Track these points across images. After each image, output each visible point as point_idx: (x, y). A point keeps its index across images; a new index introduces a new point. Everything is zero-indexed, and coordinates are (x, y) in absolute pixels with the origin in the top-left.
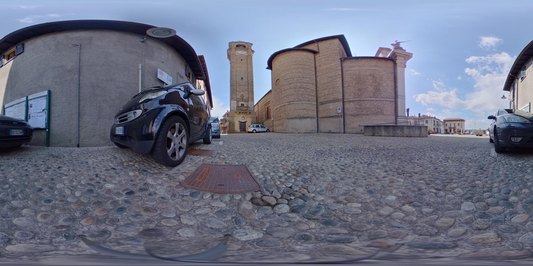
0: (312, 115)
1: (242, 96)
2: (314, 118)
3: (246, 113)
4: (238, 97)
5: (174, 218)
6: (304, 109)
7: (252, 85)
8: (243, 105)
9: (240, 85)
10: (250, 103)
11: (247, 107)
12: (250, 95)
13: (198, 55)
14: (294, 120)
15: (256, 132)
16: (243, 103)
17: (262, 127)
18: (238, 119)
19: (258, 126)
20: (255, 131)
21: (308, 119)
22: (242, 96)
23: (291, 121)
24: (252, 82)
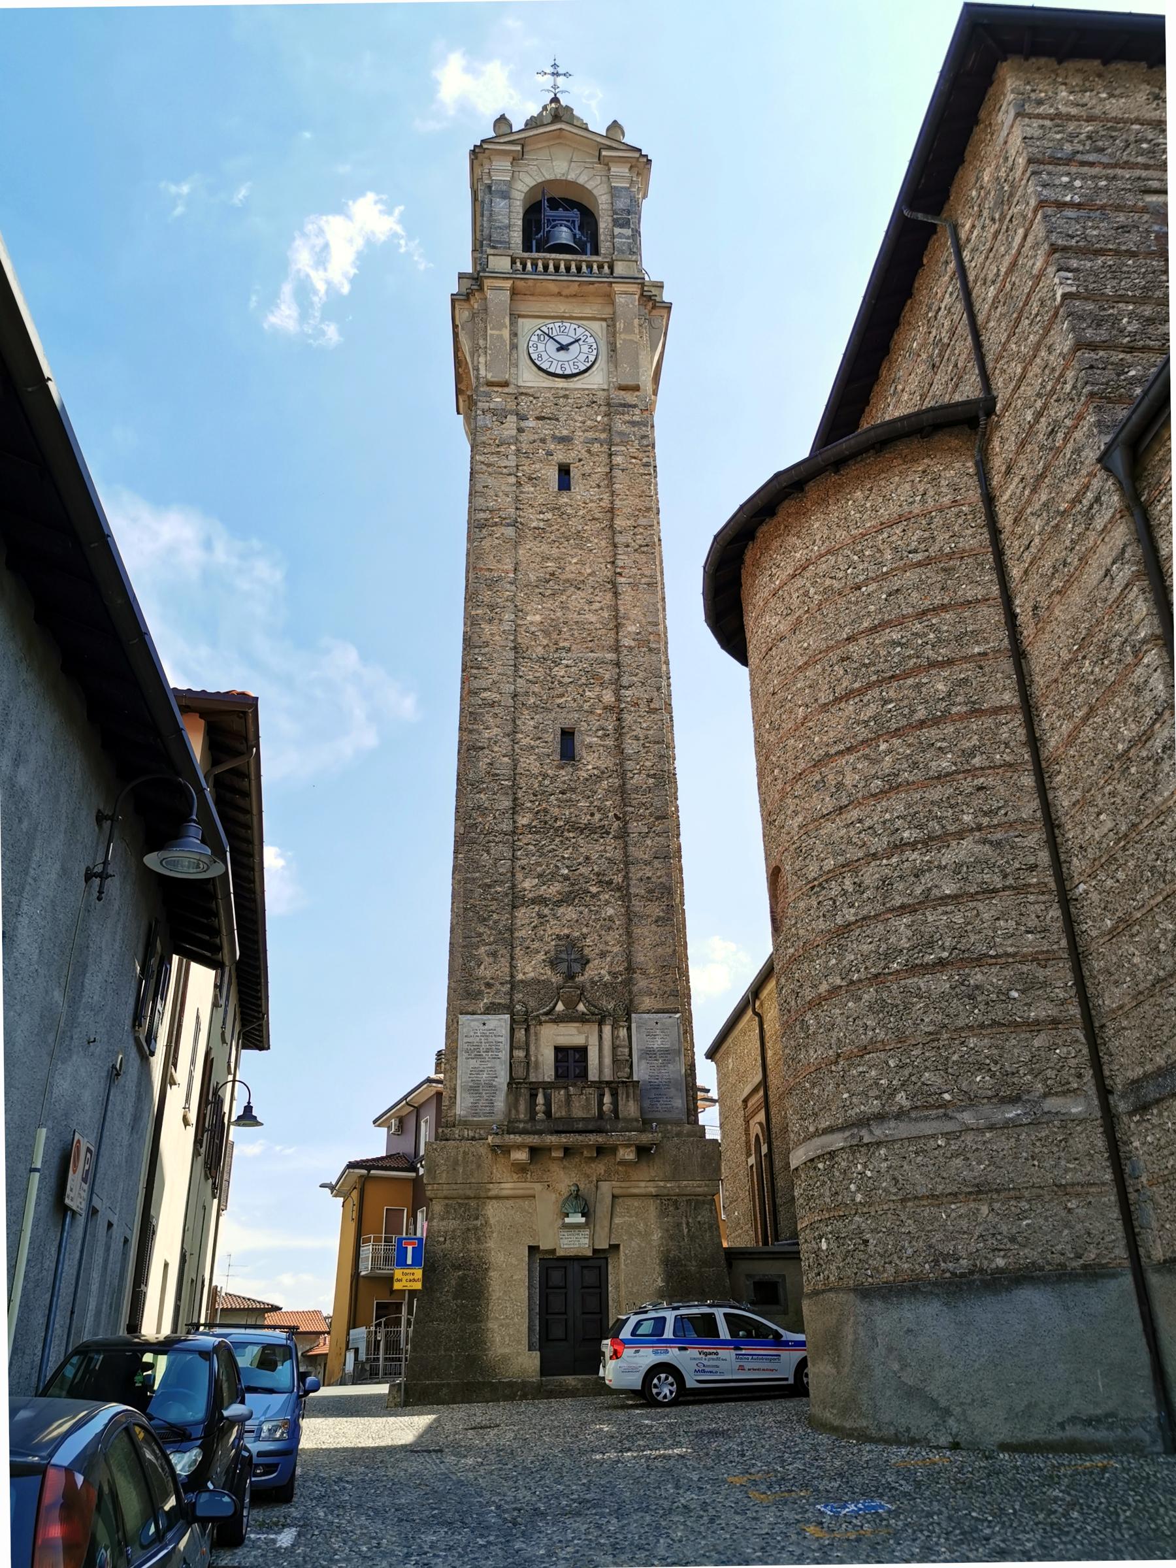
0: (1063, 1243)
1: (569, 957)
2: (1094, 1273)
4: (530, 968)
5: (637, 862)
6: (980, 1190)
7: (665, 820)
8: (571, 1060)
9: (545, 827)
10: (648, 1032)
11: (621, 1085)
12: (646, 933)
13: (176, 680)
14: (909, 1312)
15: (686, 1396)
16: (571, 1035)
17: (747, 1334)
18: (525, 1220)
19: (705, 1329)
20: (666, 1390)
21: (1031, 1297)
22: (569, 957)
23: (890, 1319)
24: (665, 780)
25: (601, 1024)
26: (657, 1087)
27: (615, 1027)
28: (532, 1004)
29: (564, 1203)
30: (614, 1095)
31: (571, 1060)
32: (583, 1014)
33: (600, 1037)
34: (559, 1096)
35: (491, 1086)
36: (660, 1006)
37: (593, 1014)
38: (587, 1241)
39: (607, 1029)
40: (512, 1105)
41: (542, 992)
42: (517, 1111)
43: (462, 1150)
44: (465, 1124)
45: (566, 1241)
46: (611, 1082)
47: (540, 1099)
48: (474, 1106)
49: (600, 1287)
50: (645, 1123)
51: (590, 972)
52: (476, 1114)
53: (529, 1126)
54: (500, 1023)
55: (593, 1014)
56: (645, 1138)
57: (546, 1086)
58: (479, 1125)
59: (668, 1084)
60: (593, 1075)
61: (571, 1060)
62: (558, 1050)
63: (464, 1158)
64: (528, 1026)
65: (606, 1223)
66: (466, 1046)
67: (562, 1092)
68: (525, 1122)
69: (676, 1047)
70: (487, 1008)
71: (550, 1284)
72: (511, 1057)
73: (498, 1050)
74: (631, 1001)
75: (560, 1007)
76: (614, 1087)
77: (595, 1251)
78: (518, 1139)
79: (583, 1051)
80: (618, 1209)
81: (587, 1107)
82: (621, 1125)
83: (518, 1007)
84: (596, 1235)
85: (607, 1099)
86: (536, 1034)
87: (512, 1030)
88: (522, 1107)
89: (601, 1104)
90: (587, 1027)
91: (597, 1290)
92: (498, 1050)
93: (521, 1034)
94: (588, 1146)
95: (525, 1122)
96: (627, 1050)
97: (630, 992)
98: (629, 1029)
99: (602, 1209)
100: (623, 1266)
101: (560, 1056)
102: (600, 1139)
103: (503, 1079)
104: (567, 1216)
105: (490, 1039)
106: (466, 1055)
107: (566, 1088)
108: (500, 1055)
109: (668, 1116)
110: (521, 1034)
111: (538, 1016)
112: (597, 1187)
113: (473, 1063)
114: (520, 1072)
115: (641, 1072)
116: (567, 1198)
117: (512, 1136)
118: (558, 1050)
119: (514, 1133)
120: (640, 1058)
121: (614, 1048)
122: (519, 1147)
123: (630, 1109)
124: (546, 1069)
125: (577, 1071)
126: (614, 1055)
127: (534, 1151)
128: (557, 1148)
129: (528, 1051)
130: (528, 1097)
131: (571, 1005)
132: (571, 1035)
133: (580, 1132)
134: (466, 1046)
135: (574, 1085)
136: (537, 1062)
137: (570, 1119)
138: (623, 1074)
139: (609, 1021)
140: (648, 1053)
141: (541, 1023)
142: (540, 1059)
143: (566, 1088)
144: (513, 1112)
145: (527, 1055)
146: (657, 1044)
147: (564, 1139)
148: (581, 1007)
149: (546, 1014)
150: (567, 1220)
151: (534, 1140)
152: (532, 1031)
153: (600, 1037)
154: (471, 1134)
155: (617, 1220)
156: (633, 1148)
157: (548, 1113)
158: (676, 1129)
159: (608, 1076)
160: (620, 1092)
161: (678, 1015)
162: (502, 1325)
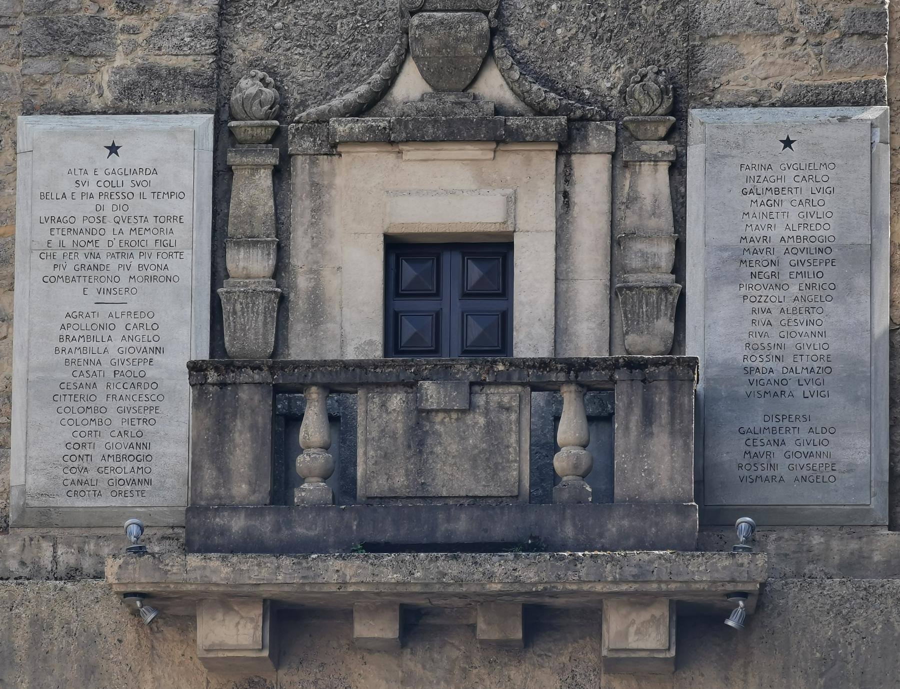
3: (542, 621)
8: (446, 286)
16: (447, 192)
25: (566, 147)
26: (777, 390)
27: (620, 162)
28: (303, 72)
30: (600, 419)
31: (446, 286)
32: (499, 110)
33: (565, 200)
34: (381, 416)
35: (139, 382)
36: (804, 76)
37: (539, 110)
39: (592, 170)
40: (210, 446)
41: (343, 27)
42: (223, 471)
43: (25, 614)
44: (44, 520)
46: (588, 364)
47: (313, 427)
48: (77, 453)
50: (713, 524)
52: (81, 486)
53: (265, 526)
54: (175, 147)
55: (539, 110)
56: (705, 572)
57: (343, 381)
58: (99, 526)
59: (821, 374)
60: (531, 339)
61: (451, 288)
62: (399, 249)
63: (35, 642)
64: (286, 159)
66: (42, 234)
67: (397, 400)
68: (255, 511)
69: (861, 235)
70: (128, 90)
72: (218, 274)
73: (169, 249)
74: (692, 58)
75: (411, 85)
76: (597, 383)
78: (217, 570)
79: (494, 253)
81: (491, 456)
82: (616, 524)
83: (248, 86)
85: (571, 426)
86: (317, 189)
87: (222, 177)
88: (244, 450)
89: (545, 446)
90: (510, 163)
92: (169, 249)
93: (254, 190)
94: (488, 600)
95: (255, 511)
96: (664, 250)
97: (689, 25)
98: (677, 168)
101: (409, 272)
102: (529, 572)
103: (185, 338)
105: (137, 207)
106: (45, 267)
107: (411, 385)
108: (175, 266)
109: (811, 497)
110: (254, 190)
111: (322, 120)
113: (73, 297)
114: (251, 333)
115: (717, 332)
117: (194, 560)
118: (399, 249)
119: (205, 549)
120: (714, 280)
121: (617, 240)
122: (229, 600)
123: (656, 464)
124: (351, 314)
125: (475, 330)
126: (615, 267)
127: (291, 622)
128: (376, 602)
129: (282, 252)
130: (263, 419)
131: (453, 75)
132: (447, 192)
133: (453, 548)
134: (42, 234)
135: (443, 374)
136: (317, 299)
137: (425, 501)
138: (647, 342)
139: (600, 138)
140: (748, 261)
141: (333, 148)
142: (332, 284)
143: (411, 385)
144: (209, 473)
145: (281, 270)
146: (784, 224)
147: (389, 571)
148: (493, 86)
149: (359, 110)
151: (278, 574)
152: (301, 170)
153: (565, 200)
154: (67, 557)
156: (661, 611)
157: (342, 476)
158: (841, 547)
159: (588, 340)
160: (620, 403)
161: (874, 113)
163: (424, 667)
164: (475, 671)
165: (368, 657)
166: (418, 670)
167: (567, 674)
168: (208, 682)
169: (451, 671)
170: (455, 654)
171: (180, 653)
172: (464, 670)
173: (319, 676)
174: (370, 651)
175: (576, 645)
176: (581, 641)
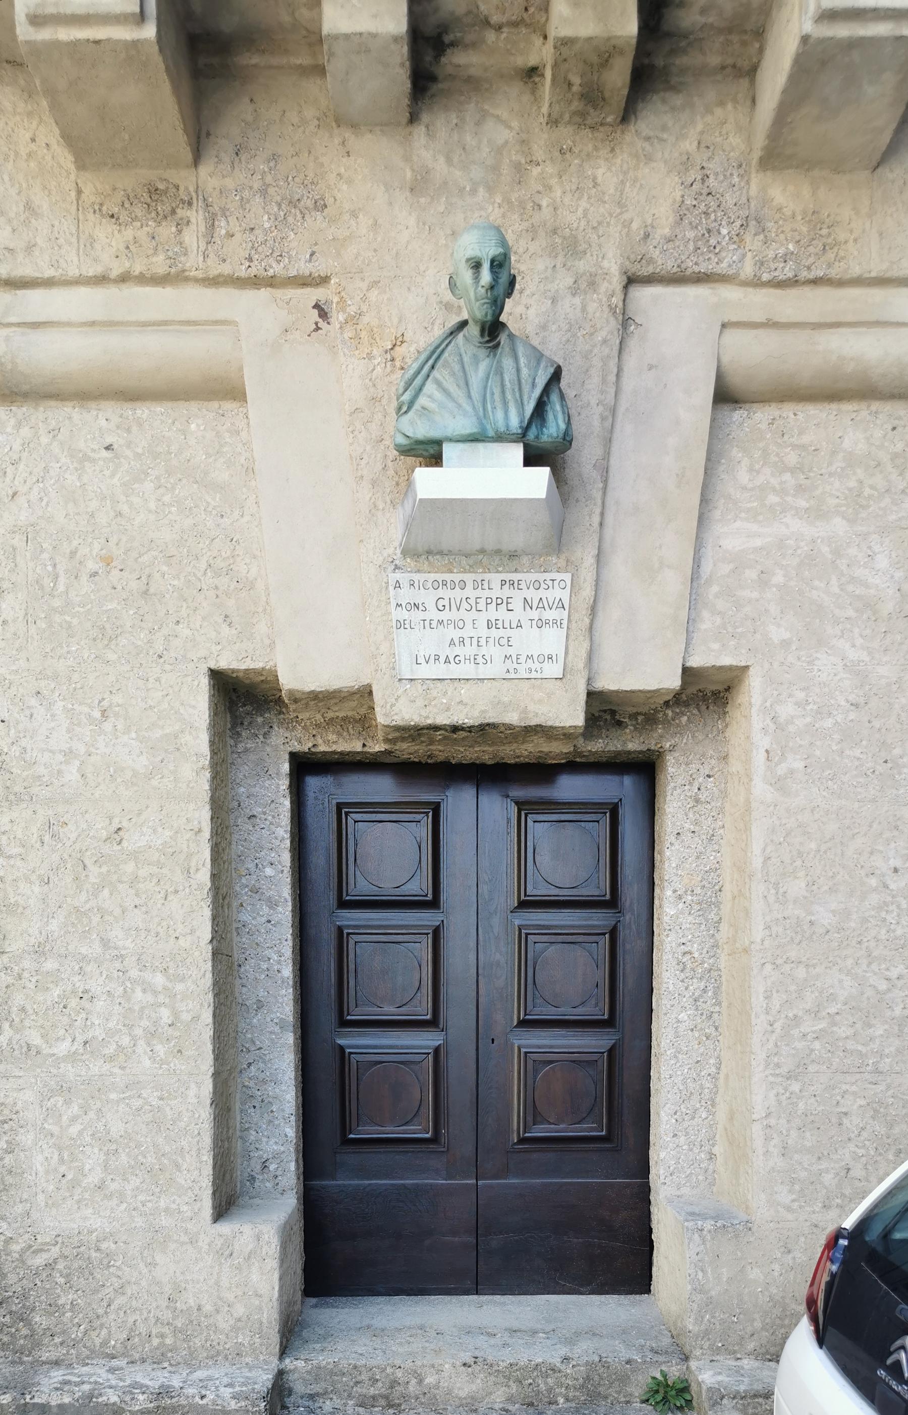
29: (414, 386)
38: (552, 641)
45: (427, 642)
49: (612, 902)
51: (427, 1381)
65: (674, 545)
71: (360, 885)
77: (604, 710)
80: (741, 475)
84: (611, 616)
91: (598, 919)
99: (652, 439)
100: (761, 789)
104: (431, 453)
112: (626, 321)
116: (435, 355)
150: (429, 482)
155: (733, 535)
162: (64, 1089)
163: (449, 160)
164: (536, 171)
165: (353, 141)
166: (440, 167)
167: (694, 174)
168: (79, 192)
169: (495, 169)
170: (503, 135)
171: (28, 136)
172: (517, 167)
173: (269, 179)
174: (354, 126)
175: (709, 119)
176: (718, 111)
